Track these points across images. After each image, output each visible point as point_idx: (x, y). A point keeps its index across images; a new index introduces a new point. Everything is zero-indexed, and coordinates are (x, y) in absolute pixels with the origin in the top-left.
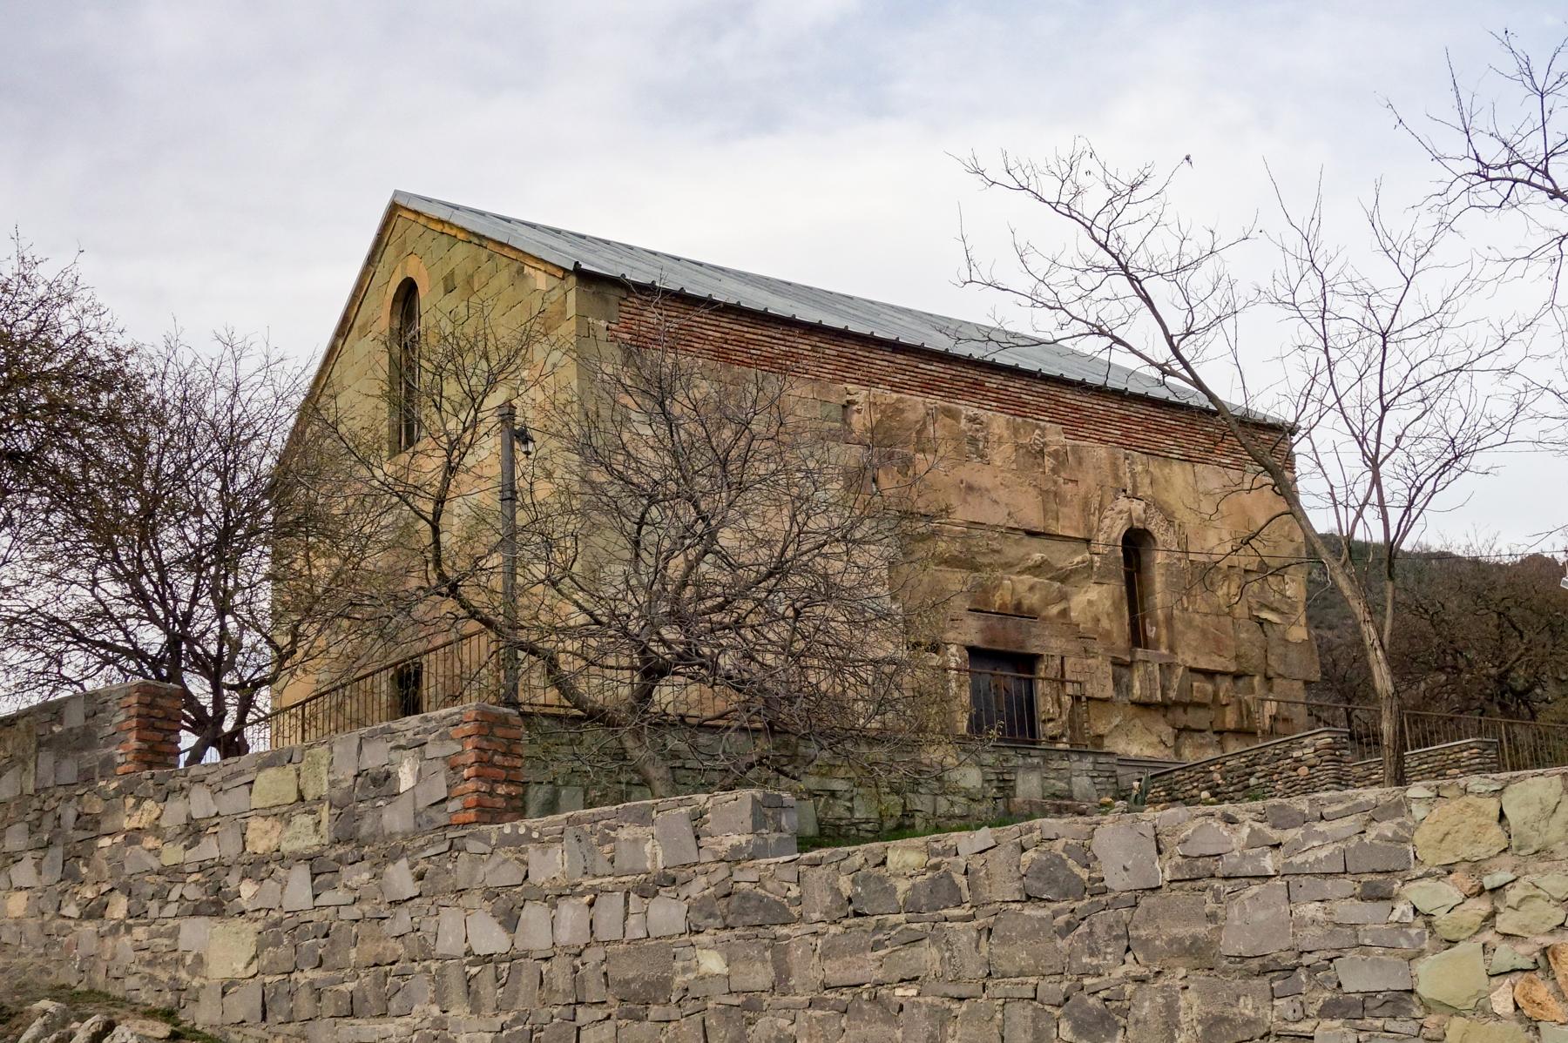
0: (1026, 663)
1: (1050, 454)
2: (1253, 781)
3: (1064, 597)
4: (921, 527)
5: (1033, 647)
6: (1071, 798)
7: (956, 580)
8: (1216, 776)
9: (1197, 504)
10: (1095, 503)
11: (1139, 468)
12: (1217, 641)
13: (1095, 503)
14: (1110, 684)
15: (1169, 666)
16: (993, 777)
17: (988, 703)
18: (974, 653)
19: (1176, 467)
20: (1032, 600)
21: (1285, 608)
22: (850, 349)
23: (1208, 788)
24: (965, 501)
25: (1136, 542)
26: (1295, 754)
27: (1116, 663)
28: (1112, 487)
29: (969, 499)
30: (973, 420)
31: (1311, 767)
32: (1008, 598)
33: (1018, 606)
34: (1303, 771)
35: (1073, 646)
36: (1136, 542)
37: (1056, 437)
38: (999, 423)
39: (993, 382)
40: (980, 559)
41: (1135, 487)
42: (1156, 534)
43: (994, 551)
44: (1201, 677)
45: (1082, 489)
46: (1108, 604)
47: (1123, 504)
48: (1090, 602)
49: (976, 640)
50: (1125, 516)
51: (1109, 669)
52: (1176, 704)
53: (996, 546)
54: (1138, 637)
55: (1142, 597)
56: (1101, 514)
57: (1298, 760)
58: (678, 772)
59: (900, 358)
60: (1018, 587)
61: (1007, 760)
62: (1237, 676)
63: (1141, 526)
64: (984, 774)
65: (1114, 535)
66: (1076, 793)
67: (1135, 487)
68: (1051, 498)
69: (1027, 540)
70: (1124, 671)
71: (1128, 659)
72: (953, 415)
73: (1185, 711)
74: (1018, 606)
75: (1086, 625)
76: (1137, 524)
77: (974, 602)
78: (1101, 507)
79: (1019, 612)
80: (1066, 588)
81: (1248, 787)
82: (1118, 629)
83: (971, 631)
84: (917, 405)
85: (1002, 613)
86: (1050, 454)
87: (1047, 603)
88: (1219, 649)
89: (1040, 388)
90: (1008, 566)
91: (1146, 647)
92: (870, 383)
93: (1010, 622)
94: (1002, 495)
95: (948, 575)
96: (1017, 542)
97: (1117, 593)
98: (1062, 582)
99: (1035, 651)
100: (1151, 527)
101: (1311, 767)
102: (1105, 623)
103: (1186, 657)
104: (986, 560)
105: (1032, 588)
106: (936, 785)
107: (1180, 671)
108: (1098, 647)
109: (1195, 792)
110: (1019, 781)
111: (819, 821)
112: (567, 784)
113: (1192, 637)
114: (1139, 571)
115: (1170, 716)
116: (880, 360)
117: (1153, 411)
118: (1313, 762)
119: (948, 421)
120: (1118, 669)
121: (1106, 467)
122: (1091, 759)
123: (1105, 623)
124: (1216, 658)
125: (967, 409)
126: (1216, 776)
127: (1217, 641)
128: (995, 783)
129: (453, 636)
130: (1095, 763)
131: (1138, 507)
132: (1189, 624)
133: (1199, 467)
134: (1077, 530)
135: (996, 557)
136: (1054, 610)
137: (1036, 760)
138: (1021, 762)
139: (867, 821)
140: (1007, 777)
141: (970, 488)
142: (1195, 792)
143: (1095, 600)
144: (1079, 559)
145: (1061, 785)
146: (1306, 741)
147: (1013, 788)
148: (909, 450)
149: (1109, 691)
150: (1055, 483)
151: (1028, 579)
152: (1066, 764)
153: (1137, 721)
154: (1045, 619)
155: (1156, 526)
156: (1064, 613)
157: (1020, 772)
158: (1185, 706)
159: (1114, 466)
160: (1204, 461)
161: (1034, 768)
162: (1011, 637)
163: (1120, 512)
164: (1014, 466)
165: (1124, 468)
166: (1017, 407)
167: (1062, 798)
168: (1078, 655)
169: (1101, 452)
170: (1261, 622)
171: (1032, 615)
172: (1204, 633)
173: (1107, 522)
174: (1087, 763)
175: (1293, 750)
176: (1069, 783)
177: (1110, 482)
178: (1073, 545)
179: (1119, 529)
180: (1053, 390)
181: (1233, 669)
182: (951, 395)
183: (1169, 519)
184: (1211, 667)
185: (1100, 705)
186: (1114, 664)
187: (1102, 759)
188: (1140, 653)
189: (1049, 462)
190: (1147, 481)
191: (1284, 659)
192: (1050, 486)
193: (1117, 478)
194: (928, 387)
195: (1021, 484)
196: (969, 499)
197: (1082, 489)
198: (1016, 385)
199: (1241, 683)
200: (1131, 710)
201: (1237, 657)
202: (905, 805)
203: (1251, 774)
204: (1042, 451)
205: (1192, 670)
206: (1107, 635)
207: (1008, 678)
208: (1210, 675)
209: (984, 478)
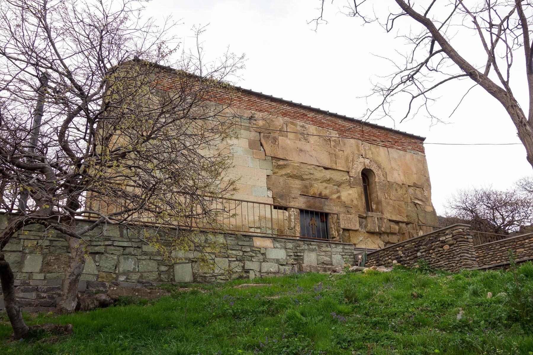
0: (324, 216)
1: (333, 141)
2: (419, 254)
3: (338, 192)
4: (281, 163)
5: (326, 210)
6: (332, 264)
7: (296, 184)
8: (400, 252)
9: (391, 164)
10: (350, 159)
11: (367, 148)
12: (399, 210)
13: (350, 159)
14: (358, 225)
15: (381, 219)
16: (292, 254)
17: (308, 230)
18: (302, 211)
19: (381, 148)
20: (326, 192)
21: (424, 200)
22: (253, 99)
23: (396, 259)
24: (299, 155)
25: (366, 174)
26: (441, 239)
27: (360, 217)
28: (357, 155)
29: (300, 154)
30: (303, 126)
31: (450, 245)
32: (316, 191)
33: (320, 194)
34: (446, 247)
35: (343, 210)
36: (366, 174)
37: (334, 134)
38: (312, 129)
39: (311, 115)
40: (305, 177)
41: (366, 154)
42: (374, 171)
43: (311, 174)
44: (393, 223)
45: (346, 153)
46: (356, 195)
47: (361, 160)
48: (349, 194)
49: (303, 207)
50: (362, 164)
51: (358, 219)
52: (384, 233)
53: (311, 172)
54: (368, 208)
55: (370, 195)
56: (353, 163)
57: (443, 242)
58: (109, 247)
59: (273, 104)
60: (318, 188)
61: (299, 246)
62: (407, 224)
63: (368, 168)
64: (287, 252)
65: (358, 170)
66: (334, 262)
67: (366, 154)
68: (334, 156)
69: (324, 170)
70: (363, 220)
71: (365, 215)
72: (295, 125)
73: (388, 236)
74: (320, 194)
75: (348, 202)
76: (367, 167)
77: (302, 192)
78: (353, 161)
79: (321, 196)
80: (339, 189)
81: (417, 257)
82: (361, 204)
83: (301, 203)
84: (280, 121)
85: (314, 197)
86: (333, 141)
87: (332, 193)
88: (400, 213)
89: (329, 118)
90: (316, 180)
91: (372, 211)
92: (260, 111)
93: (317, 200)
94: (314, 154)
95: (292, 181)
96: (320, 171)
97: (360, 191)
98: (338, 186)
99: (327, 211)
100: (372, 169)
101: (450, 245)
102: (355, 202)
103: (387, 215)
104: (308, 177)
105: (326, 188)
106: (261, 257)
107: (385, 221)
108: (353, 211)
109: (390, 261)
110: (305, 256)
111: (194, 275)
112: (31, 253)
113: (389, 208)
114: (368, 185)
115: (382, 237)
116: (265, 104)
117: (372, 130)
118: (451, 242)
119: (292, 126)
120: (361, 219)
121: (355, 147)
122: (341, 247)
123: (355, 202)
124: (398, 216)
125: (299, 123)
126: (400, 252)
127: (399, 210)
128: (293, 257)
129: (211, 237)
130: (344, 249)
131: (367, 162)
132: (388, 203)
133: (389, 149)
134: (343, 167)
135: (312, 176)
136: (335, 196)
137: (314, 247)
138: (306, 247)
139: (222, 274)
140: (299, 254)
141: (301, 150)
142: (390, 261)
143: (352, 194)
144: (344, 178)
145: (327, 259)
146: (447, 232)
147: (302, 260)
148: (276, 135)
149: (357, 227)
150: (335, 151)
151: (325, 184)
152: (329, 249)
153: (369, 239)
154: (331, 199)
155: (374, 168)
156: (339, 197)
157: (306, 252)
158: (388, 234)
159: (357, 146)
160: (392, 147)
161: (313, 250)
162: (317, 206)
163: (361, 162)
164: (318, 144)
165: (361, 148)
166: (320, 124)
167: (327, 265)
168: (345, 213)
169: (352, 141)
170: (416, 204)
171: (326, 198)
172: (394, 207)
173: (355, 166)
174: (340, 248)
175: (440, 237)
176: (331, 258)
177: (356, 152)
178: (342, 173)
179: (360, 168)
180: (334, 119)
181: (405, 220)
182: (294, 118)
183: (379, 167)
184: (397, 220)
185: (354, 232)
186: (359, 217)
187: (346, 247)
188: (370, 214)
189: (333, 144)
190: (370, 152)
191: (425, 217)
192: (333, 152)
193: (358, 150)
194: (284, 114)
195: (321, 150)
196: (300, 154)
197: (346, 153)
198: (319, 117)
199: (409, 226)
200: (367, 235)
201: (407, 216)
202: (243, 267)
203: (418, 251)
204: (329, 139)
205: (390, 221)
206: (356, 206)
207: (317, 222)
208: (397, 222)
209: (307, 147)
